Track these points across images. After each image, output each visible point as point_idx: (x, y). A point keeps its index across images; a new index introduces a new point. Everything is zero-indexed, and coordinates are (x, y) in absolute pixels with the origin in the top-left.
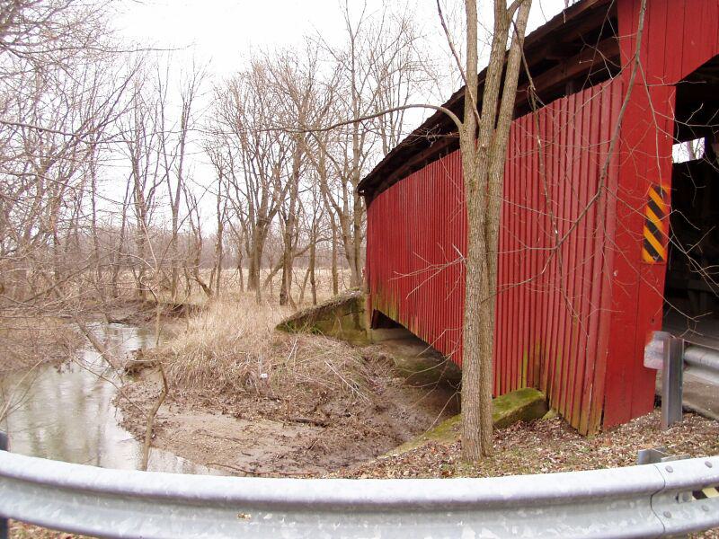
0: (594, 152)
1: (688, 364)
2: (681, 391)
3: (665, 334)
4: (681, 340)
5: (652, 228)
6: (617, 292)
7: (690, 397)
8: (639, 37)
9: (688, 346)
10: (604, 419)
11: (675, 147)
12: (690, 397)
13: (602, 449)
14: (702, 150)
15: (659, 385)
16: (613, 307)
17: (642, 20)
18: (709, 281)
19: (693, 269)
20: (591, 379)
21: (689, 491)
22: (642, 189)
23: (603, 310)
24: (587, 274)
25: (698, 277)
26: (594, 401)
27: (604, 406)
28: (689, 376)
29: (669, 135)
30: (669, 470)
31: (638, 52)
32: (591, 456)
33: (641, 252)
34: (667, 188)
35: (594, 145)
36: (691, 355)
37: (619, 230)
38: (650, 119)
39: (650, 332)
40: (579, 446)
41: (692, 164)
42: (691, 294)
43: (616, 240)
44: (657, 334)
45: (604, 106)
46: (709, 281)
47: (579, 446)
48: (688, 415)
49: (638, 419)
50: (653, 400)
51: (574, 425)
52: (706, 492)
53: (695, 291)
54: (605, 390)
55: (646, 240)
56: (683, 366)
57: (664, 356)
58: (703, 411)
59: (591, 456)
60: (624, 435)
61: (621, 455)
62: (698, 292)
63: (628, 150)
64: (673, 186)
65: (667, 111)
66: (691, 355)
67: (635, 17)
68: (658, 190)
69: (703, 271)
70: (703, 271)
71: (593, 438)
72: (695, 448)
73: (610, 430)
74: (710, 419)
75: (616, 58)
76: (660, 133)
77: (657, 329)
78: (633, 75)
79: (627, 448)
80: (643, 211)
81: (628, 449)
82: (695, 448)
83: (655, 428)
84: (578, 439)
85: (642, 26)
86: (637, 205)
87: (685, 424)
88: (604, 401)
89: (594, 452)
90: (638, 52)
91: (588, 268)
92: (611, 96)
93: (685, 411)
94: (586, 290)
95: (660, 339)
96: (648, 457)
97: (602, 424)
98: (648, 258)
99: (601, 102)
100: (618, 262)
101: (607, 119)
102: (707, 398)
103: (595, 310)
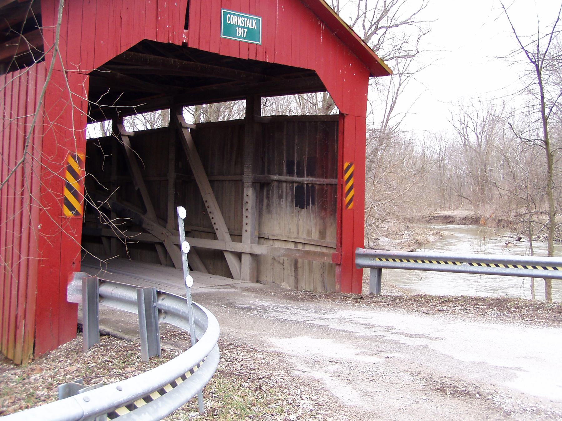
0: (21, 124)
1: (102, 297)
2: (97, 319)
3: (83, 274)
4: (95, 279)
5: (70, 188)
6: (41, 242)
7: (104, 322)
8: (58, 29)
9: (102, 282)
10: (36, 348)
11: (90, 127)
12: (104, 322)
13: (33, 377)
14: (111, 130)
15: (80, 314)
16: (39, 256)
17: (60, 15)
18: (115, 229)
19: (104, 221)
20: (23, 317)
21: (104, 414)
22: (61, 155)
23: (31, 258)
24: (17, 228)
25: (107, 227)
26: (27, 335)
27: (35, 337)
28: (104, 306)
29: (85, 114)
30: (86, 400)
31: (57, 41)
32: (24, 385)
33: (350, 210)
34: (83, 156)
35: (22, 116)
36: (104, 289)
37: (42, 190)
38: (67, 98)
39: (71, 273)
40: (13, 377)
41: (104, 140)
42: (104, 240)
43: (41, 199)
44: (77, 274)
45: (30, 86)
46: (115, 229)
47: (13, 377)
48: (104, 337)
49: (65, 345)
50: (76, 328)
51: (10, 356)
52: (118, 411)
53: (106, 237)
54: (36, 323)
55: (66, 199)
56: (98, 299)
57: (83, 291)
58: (115, 333)
59: (24, 385)
60: (53, 360)
61: (50, 380)
62: (109, 238)
63: (49, 124)
64: (87, 154)
65: (82, 94)
66: (104, 289)
67: (55, 13)
68: (74, 157)
69: (112, 223)
70: (112, 223)
71: (27, 366)
72: (110, 364)
73: (41, 357)
74: (121, 339)
75: (41, 48)
76: (75, 110)
77: (77, 270)
78: (53, 61)
79: (56, 372)
80: (63, 174)
81: (56, 373)
82: (110, 364)
83: (78, 351)
84: (13, 369)
85: (61, 20)
86: (56, 168)
87: (102, 346)
88: (35, 333)
89: (27, 381)
90: (57, 41)
91: (17, 222)
92: (36, 77)
93: (102, 335)
94: (16, 241)
95: (80, 278)
96: (68, 389)
97: (34, 353)
98: (67, 213)
99: (28, 83)
100: (43, 218)
101: (33, 98)
102: (118, 322)
103: (24, 258)
